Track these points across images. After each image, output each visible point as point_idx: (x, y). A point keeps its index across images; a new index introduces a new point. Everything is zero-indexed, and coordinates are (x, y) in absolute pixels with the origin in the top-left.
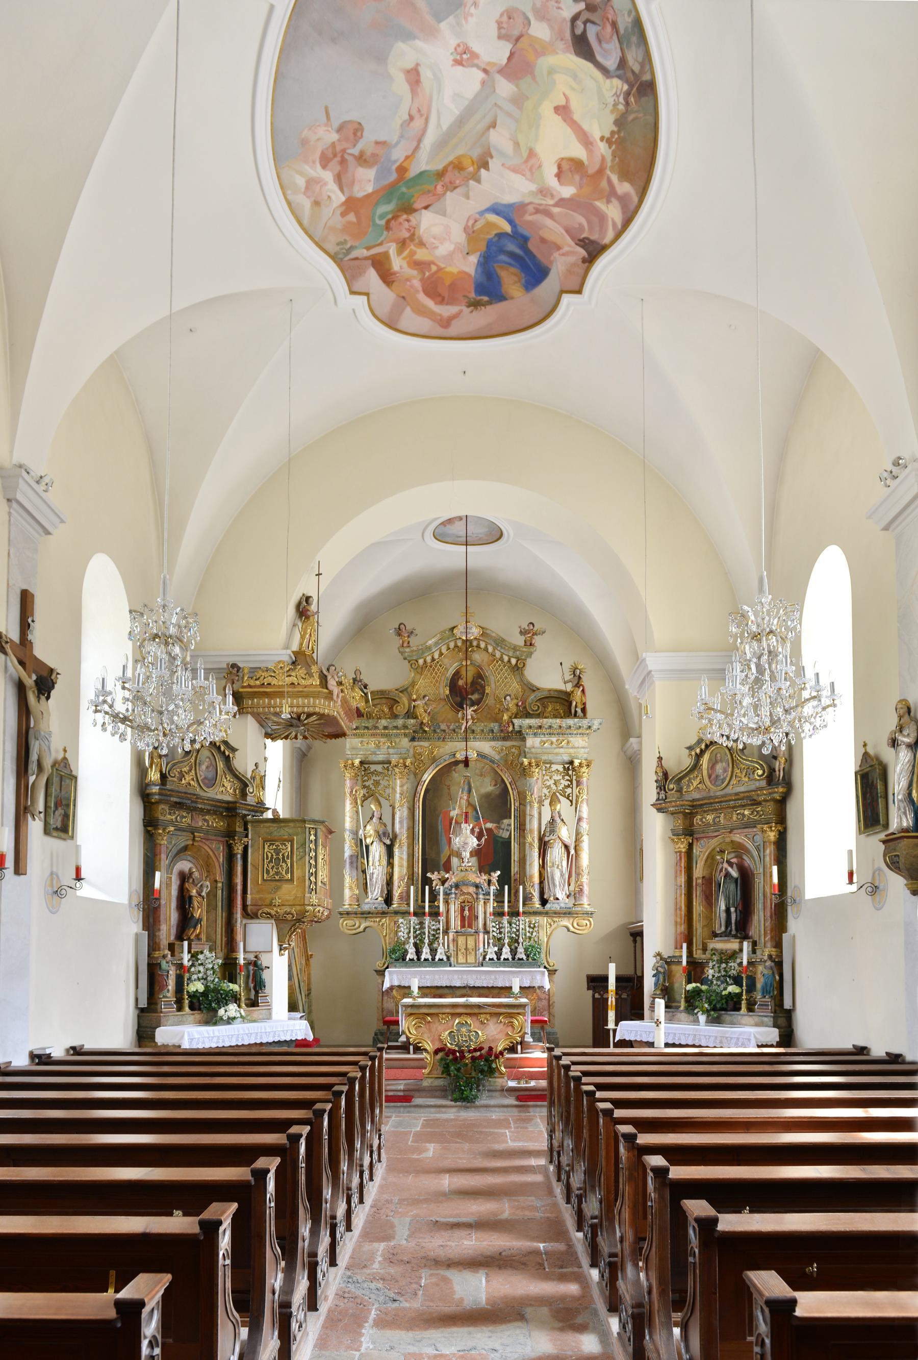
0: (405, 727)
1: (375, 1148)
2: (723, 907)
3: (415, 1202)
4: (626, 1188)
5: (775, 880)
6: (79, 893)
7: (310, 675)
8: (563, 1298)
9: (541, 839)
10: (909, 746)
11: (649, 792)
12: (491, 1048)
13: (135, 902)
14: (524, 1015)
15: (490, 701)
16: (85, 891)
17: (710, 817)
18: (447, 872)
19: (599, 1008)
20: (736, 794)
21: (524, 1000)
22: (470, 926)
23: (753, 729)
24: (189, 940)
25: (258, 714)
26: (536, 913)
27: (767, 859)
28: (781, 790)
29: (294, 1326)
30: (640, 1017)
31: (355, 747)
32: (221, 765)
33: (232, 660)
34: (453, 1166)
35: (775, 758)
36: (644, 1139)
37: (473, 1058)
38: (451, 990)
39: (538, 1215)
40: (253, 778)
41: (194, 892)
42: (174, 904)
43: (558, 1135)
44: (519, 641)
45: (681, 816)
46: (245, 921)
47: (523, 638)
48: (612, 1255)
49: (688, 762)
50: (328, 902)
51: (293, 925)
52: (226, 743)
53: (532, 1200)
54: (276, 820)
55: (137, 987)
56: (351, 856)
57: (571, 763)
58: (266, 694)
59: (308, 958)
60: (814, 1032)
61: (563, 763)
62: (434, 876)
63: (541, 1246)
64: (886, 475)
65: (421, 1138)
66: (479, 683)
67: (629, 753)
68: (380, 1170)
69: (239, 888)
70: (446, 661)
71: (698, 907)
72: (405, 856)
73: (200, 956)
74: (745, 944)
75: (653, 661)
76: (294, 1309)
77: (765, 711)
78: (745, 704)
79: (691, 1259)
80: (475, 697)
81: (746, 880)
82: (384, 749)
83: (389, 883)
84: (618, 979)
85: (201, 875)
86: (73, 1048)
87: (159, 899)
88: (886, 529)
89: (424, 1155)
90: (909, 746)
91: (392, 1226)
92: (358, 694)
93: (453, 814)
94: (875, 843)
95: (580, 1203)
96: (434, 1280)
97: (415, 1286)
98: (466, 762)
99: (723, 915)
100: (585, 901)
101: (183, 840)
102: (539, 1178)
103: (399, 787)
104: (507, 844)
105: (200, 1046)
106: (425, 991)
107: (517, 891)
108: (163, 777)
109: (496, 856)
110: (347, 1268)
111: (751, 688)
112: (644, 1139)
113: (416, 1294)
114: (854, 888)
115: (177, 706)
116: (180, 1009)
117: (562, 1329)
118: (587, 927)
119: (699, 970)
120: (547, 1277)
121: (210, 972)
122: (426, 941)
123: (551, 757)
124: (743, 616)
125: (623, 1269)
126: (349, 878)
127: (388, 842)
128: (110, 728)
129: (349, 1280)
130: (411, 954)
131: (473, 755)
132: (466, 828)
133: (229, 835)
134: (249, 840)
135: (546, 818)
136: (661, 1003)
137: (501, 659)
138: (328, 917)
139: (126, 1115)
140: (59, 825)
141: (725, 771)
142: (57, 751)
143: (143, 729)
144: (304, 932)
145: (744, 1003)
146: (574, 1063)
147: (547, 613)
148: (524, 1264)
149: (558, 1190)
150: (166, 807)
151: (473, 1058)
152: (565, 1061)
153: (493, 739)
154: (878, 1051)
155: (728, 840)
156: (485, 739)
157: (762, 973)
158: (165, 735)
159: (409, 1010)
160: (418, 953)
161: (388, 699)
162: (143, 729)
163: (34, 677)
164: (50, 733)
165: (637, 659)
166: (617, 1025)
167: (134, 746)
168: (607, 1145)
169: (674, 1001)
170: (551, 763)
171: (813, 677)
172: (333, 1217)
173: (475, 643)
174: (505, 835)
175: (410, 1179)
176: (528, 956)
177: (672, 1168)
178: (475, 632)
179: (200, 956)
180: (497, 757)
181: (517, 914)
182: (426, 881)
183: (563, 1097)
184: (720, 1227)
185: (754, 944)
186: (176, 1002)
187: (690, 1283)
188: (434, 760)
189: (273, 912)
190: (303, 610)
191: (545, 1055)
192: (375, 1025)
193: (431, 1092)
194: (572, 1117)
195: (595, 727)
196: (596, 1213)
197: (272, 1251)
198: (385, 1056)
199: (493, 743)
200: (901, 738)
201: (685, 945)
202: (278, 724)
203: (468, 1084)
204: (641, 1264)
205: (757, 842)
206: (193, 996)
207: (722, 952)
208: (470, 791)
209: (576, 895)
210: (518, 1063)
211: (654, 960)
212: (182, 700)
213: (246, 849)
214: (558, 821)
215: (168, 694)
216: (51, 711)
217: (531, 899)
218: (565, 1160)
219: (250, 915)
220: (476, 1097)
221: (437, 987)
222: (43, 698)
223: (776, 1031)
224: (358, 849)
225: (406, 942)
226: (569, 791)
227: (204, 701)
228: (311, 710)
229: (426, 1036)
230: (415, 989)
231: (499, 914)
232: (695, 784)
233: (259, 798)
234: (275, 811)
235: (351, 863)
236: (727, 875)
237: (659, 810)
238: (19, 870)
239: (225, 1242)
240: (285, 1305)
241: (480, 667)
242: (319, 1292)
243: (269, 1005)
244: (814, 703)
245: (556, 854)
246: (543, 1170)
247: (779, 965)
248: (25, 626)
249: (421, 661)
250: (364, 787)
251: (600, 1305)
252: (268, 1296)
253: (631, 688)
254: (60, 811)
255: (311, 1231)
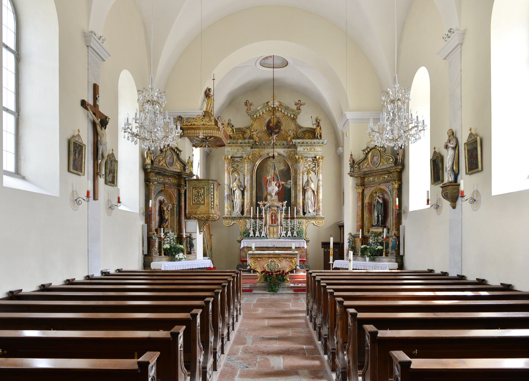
0: (249, 143)
1: (238, 309)
2: (376, 215)
3: (254, 330)
4: (339, 322)
5: (397, 204)
6: (119, 208)
7: (211, 121)
8: (313, 366)
9: (303, 188)
10: (453, 148)
11: (347, 168)
12: (283, 271)
13: (142, 212)
14: (296, 258)
15: (283, 132)
16: (121, 207)
17: (371, 179)
18: (266, 201)
19: (326, 255)
20: (382, 169)
21: (296, 252)
22: (275, 223)
23: (391, 140)
24: (163, 227)
25: (190, 137)
26: (301, 218)
27: (394, 195)
28: (400, 167)
29: (208, 376)
30: (343, 259)
31: (229, 151)
32: (175, 157)
33: (179, 115)
34: (269, 316)
35: (398, 154)
36: (346, 303)
37: (276, 275)
38: (268, 248)
39: (303, 335)
40: (188, 163)
41: (165, 209)
42: (157, 214)
43: (311, 304)
44: (295, 108)
45: (360, 178)
46: (185, 220)
47: (296, 106)
48: (333, 349)
49: (362, 156)
50: (218, 213)
51: (205, 222)
52: (177, 148)
53: (300, 329)
54: (197, 180)
55: (143, 246)
56: (227, 195)
57: (315, 157)
58: (193, 129)
59: (211, 236)
60: (411, 265)
61: (312, 158)
62: (260, 203)
63: (304, 346)
64: (445, 36)
65: (256, 306)
66: (278, 125)
67: (338, 154)
68: (240, 318)
69: (183, 207)
70: (265, 116)
71: (366, 215)
72: (249, 195)
73: (168, 234)
74: (385, 229)
75: (349, 115)
76: (208, 369)
77: (396, 132)
78: (388, 129)
79: (367, 348)
80: (277, 131)
81: (385, 204)
82: (240, 152)
83: (243, 206)
84: (334, 244)
85: (168, 201)
86: (118, 270)
87: (151, 211)
88: (445, 59)
89: (257, 312)
90: (453, 148)
91: (245, 339)
92: (230, 129)
93: (268, 178)
94: (438, 188)
95: (320, 330)
96: (262, 359)
97: (255, 362)
98: (273, 157)
99: (376, 218)
100: (321, 213)
101: (161, 187)
102: (303, 321)
103: (246, 167)
104: (290, 190)
105: (168, 269)
106: (257, 248)
107: (294, 209)
108: (152, 162)
109: (285, 195)
110: (228, 355)
111: (391, 123)
112: (346, 303)
113: (255, 365)
114: (429, 206)
115: (157, 129)
116: (160, 255)
117: (313, 378)
118: (322, 224)
119: (366, 240)
120: (307, 358)
121: (172, 241)
122: (258, 229)
123: (307, 155)
124: (387, 93)
125: (338, 354)
126: (227, 204)
127: (242, 189)
128: (130, 139)
129: (229, 359)
130: (252, 234)
131: (276, 154)
132: (274, 183)
133: (179, 185)
134: (187, 188)
135: (305, 180)
136: (351, 253)
137: (287, 115)
138: (219, 219)
139: (139, 293)
140: (111, 180)
141: (378, 160)
142: (109, 150)
143: (144, 139)
144: (209, 225)
145: (384, 253)
146: (317, 276)
147: (306, 96)
148: (298, 353)
149: (311, 325)
150: (154, 174)
151: (276, 275)
152: (313, 275)
153: (284, 148)
154: (438, 271)
155: (378, 188)
156: (281, 148)
157: (391, 241)
158: (153, 142)
159: (251, 256)
160: (254, 234)
161: (242, 132)
162: (144, 139)
163: (99, 120)
164: (106, 143)
165: (342, 114)
166: (333, 262)
167: (140, 147)
168: (331, 306)
169: (356, 252)
170: (307, 158)
171: (416, 118)
172: (223, 335)
173: (277, 109)
174: (289, 186)
175: (252, 321)
176: (298, 235)
177: (358, 314)
178: (277, 104)
179: (168, 234)
180: (286, 155)
181: (294, 218)
182: (257, 205)
183: (313, 289)
184: (379, 335)
185: (388, 229)
186: (159, 252)
187: (366, 358)
188: (260, 156)
189: (197, 217)
190: (208, 94)
191: (305, 274)
192: (237, 262)
193: (260, 288)
194: (317, 296)
195: (325, 143)
196: (327, 333)
197: (199, 347)
198: (242, 274)
199: (284, 150)
200: (449, 145)
201: (361, 230)
202: (198, 141)
203: (275, 285)
204: (345, 352)
205: (391, 188)
206: (165, 250)
207: (375, 233)
208: (275, 169)
209: (317, 211)
210: (294, 277)
211: (348, 236)
212: (160, 127)
213: (185, 191)
214: (310, 181)
215: (154, 124)
216: (106, 134)
217: (299, 212)
218: (313, 313)
219: (187, 218)
220: (278, 290)
221: (262, 247)
222: (103, 128)
223: (397, 264)
224: (231, 193)
225: (250, 229)
226: (314, 169)
227: (168, 128)
228: (211, 135)
229: (258, 266)
230: (254, 248)
231: (286, 218)
232: (365, 165)
233: (191, 170)
234: (197, 176)
235: (228, 198)
236: (378, 202)
237: (351, 176)
238: (95, 198)
239: (181, 341)
240: (204, 368)
241: (278, 118)
242: (217, 364)
243: (195, 253)
244: (416, 129)
245: (309, 194)
246: (305, 318)
247: (398, 238)
248: (95, 99)
249: (255, 116)
250: (233, 167)
251: (328, 369)
252: (198, 364)
253: (340, 126)
254: (111, 175)
255: (214, 340)
